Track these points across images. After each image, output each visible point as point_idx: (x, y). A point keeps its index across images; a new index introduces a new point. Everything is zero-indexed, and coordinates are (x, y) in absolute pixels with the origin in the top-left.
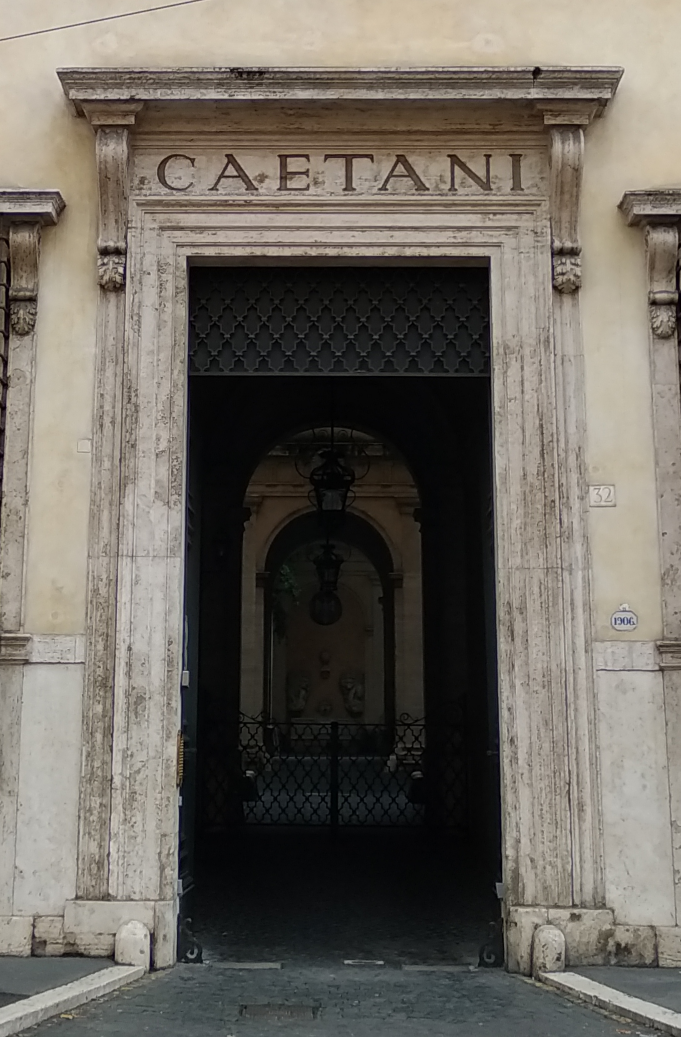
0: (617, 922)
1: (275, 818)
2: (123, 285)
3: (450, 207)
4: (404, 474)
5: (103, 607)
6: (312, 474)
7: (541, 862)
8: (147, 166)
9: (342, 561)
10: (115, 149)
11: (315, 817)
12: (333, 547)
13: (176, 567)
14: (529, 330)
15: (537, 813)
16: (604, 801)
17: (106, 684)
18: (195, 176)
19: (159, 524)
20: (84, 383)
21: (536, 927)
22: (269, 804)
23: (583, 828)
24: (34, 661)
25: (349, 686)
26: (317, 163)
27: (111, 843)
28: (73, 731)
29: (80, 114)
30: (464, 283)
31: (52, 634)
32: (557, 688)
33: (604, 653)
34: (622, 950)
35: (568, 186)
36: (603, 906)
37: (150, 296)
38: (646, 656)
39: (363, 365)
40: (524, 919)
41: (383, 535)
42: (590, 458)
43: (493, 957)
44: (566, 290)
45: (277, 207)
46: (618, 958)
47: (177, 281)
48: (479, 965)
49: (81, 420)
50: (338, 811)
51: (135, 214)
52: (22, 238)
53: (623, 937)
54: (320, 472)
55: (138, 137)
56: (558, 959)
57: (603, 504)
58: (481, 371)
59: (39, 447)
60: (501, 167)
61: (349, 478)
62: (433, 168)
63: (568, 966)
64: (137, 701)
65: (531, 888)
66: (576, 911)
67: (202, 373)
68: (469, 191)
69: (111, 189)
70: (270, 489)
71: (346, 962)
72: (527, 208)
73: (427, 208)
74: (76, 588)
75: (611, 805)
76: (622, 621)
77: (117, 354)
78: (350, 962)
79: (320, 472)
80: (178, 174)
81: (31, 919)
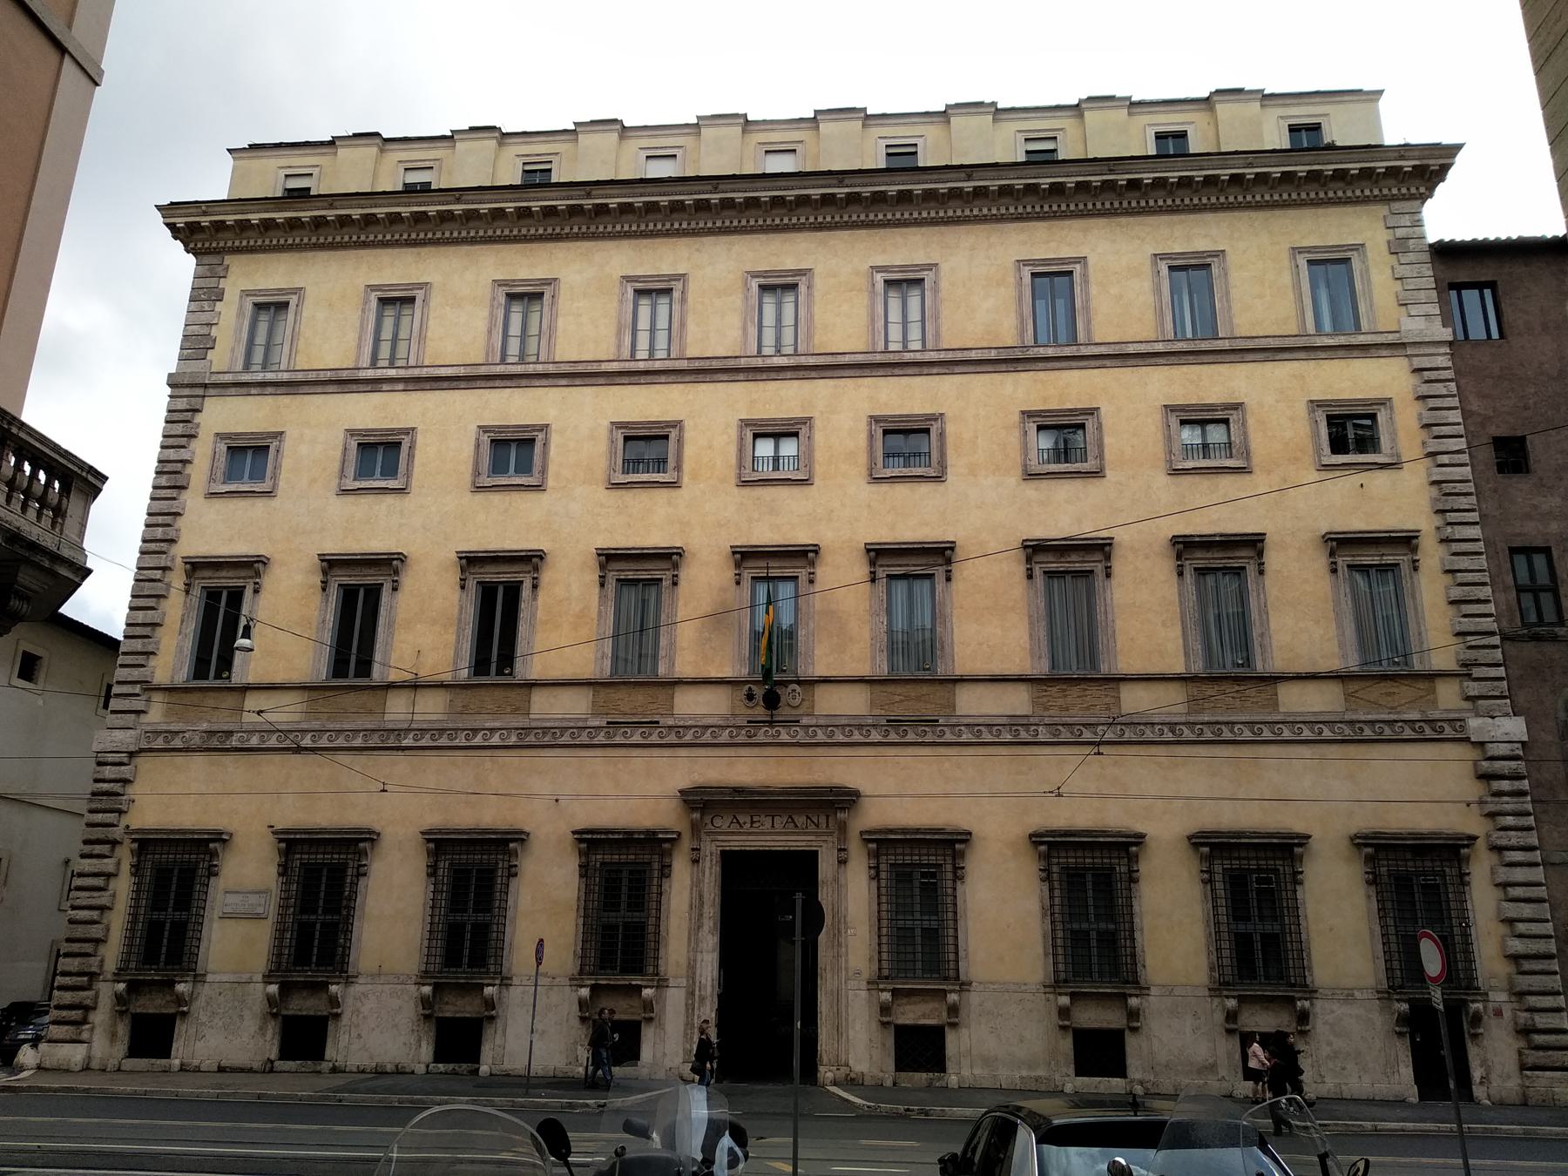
3: (805, 834)
5: (692, 967)
8: (707, 819)
10: (696, 815)
13: (716, 956)
14: (830, 876)
17: (693, 993)
18: (723, 823)
19: (710, 942)
20: (686, 895)
22: (1349, 426)
24: (820, 671)
26: (763, 818)
28: (683, 1009)
30: (810, 858)
31: (676, 977)
32: (837, 996)
33: (852, 984)
34: (852, 1080)
35: (843, 828)
37: (708, 864)
38: (864, 985)
40: (821, 1069)
42: (849, 919)
44: (842, 862)
45: (750, 834)
46: (851, 1083)
47: (716, 858)
49: (686, 907)
51: (703, 837)
52: (666, 846)
59: (672, 917)
60: (823, 820)
62: (801, 820)
63: (835, 1083)
64: (702, 999)
65: (825, 1060)
68: (812, 828)
69: (696, 829)
72: (831, 834)
73: (798, 834)
74: (683, 961)
75: (851, 1033)
77: (697, 884)
80: (718, 822)
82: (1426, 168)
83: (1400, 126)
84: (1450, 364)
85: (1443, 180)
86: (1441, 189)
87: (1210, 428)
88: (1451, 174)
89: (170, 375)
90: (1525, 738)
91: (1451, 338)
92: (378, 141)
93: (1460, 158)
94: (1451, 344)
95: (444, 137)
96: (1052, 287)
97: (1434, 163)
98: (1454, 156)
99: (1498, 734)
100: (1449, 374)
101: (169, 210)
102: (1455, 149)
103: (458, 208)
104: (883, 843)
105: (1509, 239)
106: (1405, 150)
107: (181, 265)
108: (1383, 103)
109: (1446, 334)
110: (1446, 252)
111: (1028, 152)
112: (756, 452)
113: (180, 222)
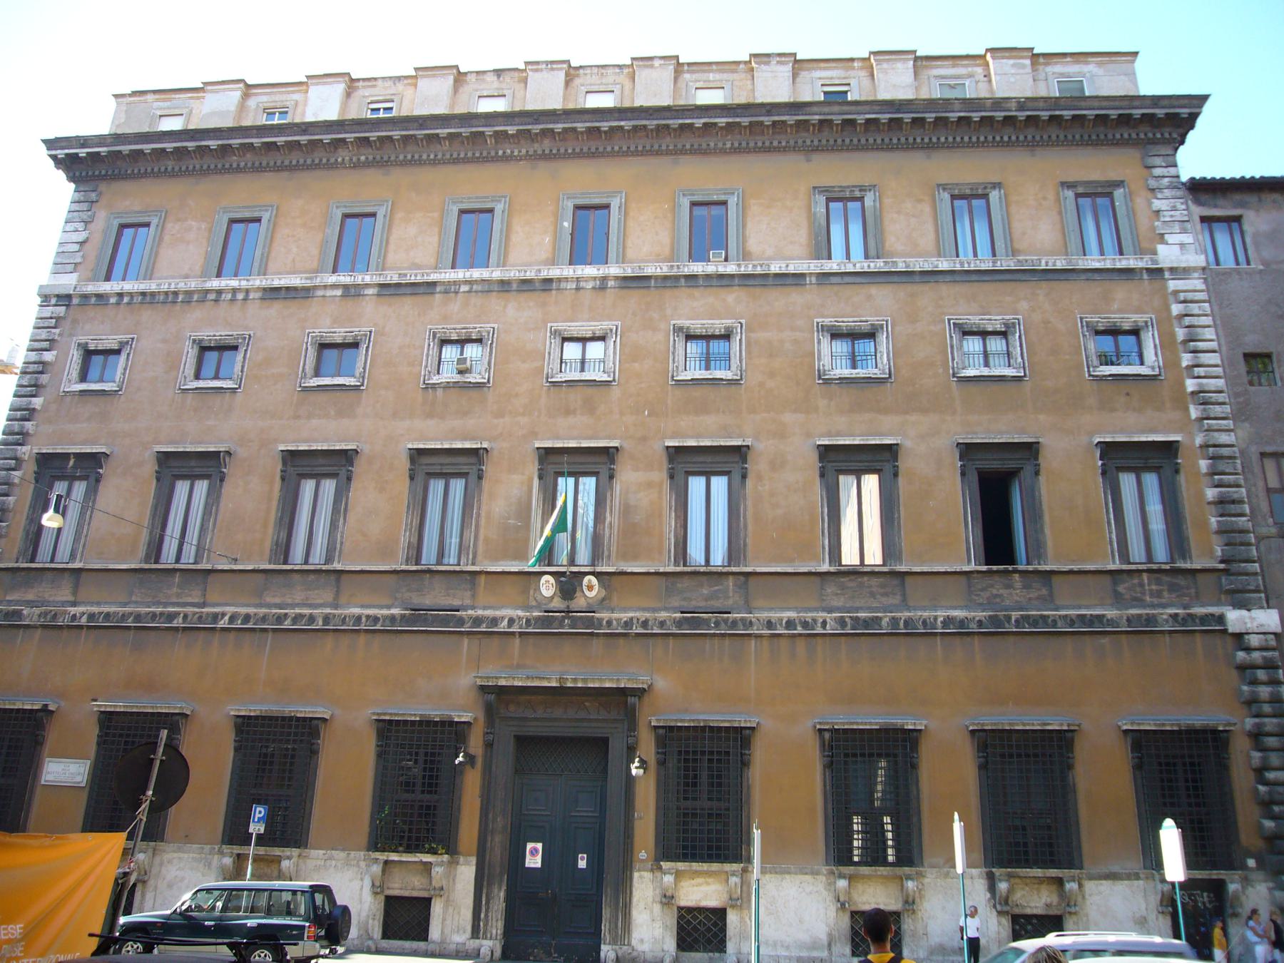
82: (1173, 119)
83: (1155, 79)
84: (1203, 287)
85: (1192, 127)
86: (1191, 135)
87: (1120, 338)
88: (1200, 122)
89: (41, 287)
90: (1279, 630)
91: (1204, 264)
92: (241, 85)
93: (1207, 109)
94: (1204, 269)
95: (300, 83)
96: (845, 209)
97: (1184, 112)
98: (1201, 106)
99: (1251, 626)
100: (1203, 296)
101: (50, 144)
102: (1203, 99)
103: (303, 139)
104: (668, 736)
105: (1253, 178)
106: (1156, 100)
107: (62, 189)
108: (1139, 64)
109: (1198, 260)
110: (1202, 189)
111: (825, 93)
112: (553, 329)
113: (61, 153)
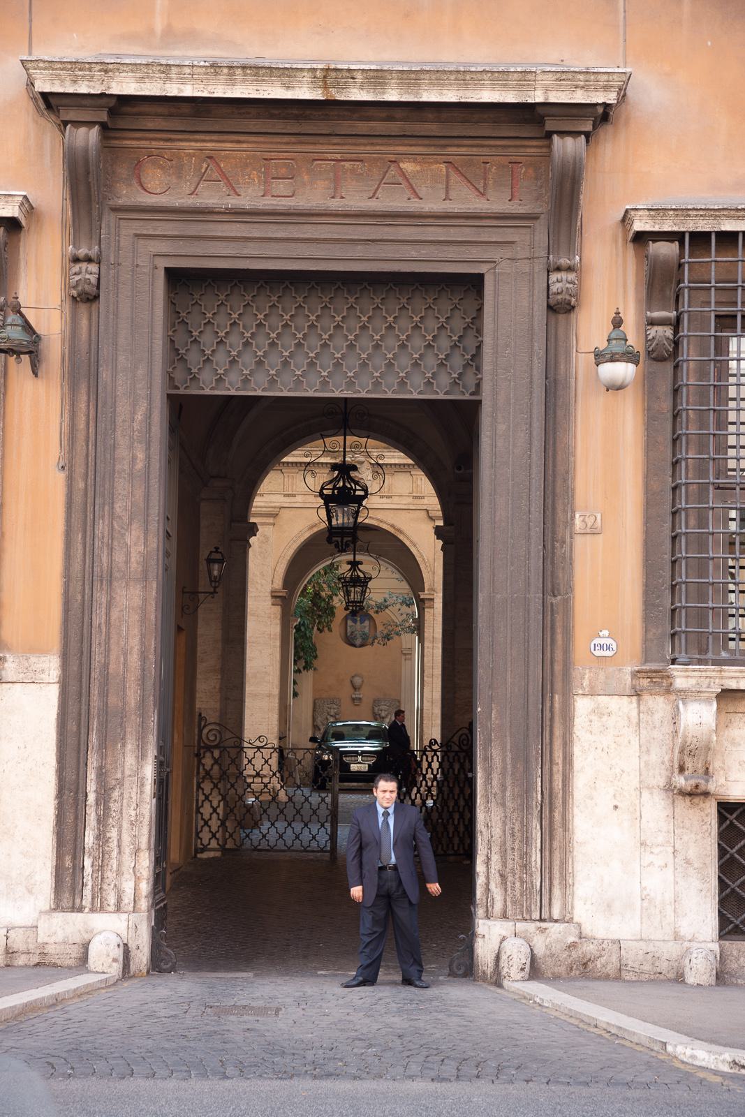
0: (583, 935)
1: (256, 843)
2: (97, 297)
4: (424, 485)
6: (322, 488)
7: (510, 878)
9: (371, 579)
11: (314, 844)
12: (361, 563)
15: (508, 832)
16: (575, 820)
21: (503, 939)
23: (554, 846)
25: (383, 714)
27: (86, 858)
29: (49, 106)
35: (565, 196)
36: (570, 921)
39: (350, 384)
41: (413, 550)
43: (463, 968)
48: (449, 975)
50: (330, 839)
53: (590, 949)
54: (330, 486)
55: (112, 134)
56: (522, 969)
57: (588, 531)
58: (472, 394)
61: (362, 493)
66: (544, 925)
67: (182, 391)
70: (287, 499)
71: (319, 973)
76: (602, 647)
78: (321, 972)
79: (330, 486)
81: (5, 930)
